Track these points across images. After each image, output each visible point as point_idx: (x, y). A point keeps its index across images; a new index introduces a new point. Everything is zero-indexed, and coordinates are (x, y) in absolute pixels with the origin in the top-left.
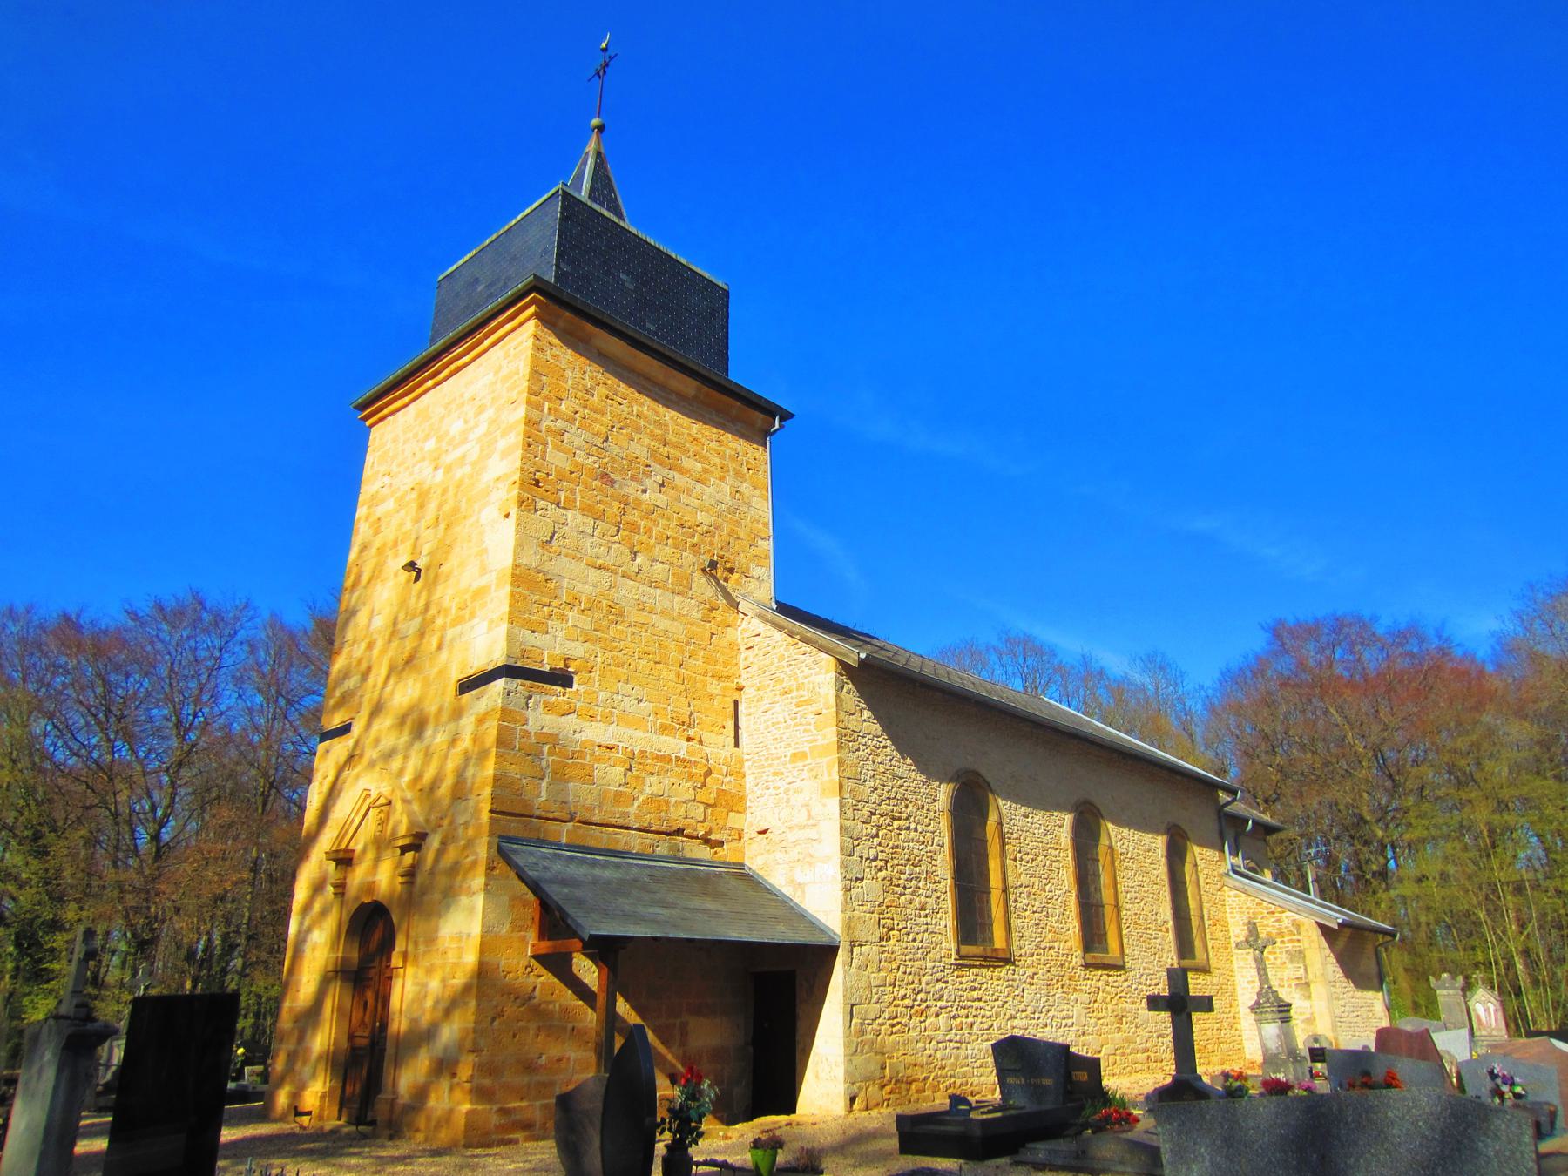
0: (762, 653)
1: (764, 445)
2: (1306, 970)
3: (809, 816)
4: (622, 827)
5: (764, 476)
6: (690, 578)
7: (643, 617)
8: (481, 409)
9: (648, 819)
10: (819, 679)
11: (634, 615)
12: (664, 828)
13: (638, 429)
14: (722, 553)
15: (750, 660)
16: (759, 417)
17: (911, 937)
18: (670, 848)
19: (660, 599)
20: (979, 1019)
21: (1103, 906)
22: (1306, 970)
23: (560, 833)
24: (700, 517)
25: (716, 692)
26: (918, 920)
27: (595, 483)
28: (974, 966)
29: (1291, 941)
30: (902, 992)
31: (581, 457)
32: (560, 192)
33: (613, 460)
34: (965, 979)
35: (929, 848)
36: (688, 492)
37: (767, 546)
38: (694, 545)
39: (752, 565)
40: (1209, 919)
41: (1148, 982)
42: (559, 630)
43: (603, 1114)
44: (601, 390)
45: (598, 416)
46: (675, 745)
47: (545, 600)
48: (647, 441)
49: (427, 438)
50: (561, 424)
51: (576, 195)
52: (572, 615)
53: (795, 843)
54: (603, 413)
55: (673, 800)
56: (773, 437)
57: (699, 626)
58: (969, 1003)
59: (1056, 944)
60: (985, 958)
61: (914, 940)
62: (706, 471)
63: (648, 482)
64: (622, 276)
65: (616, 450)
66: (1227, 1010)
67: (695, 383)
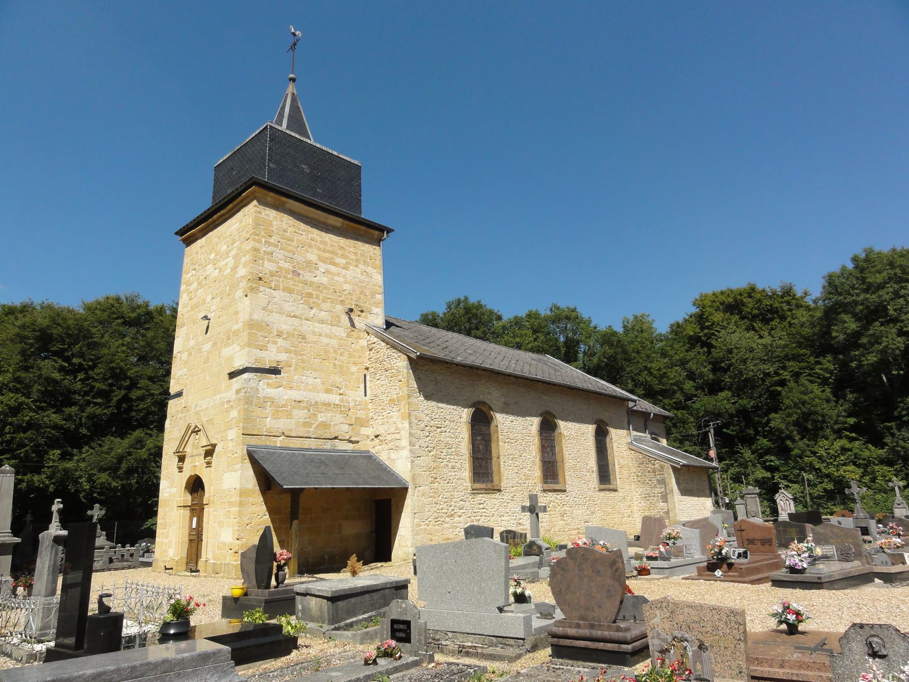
0: (376, 352)
1: (379, 246)
2: (666, 489)
3: (397, 429)
4: (307, 438)
5: (379, 262)
6: (339, 317)
7: (315, 338)
8: (234, 241)
9: (320, 433)
10: (400, 364)
11: (310, 338)
12: (328, 436)
13: (310, 246)
14: (357, 303)
15: (372, 354)
16: (376, 233)
17: (446, 482)
18: (331, 446)
19: (326, 329)
20: (483, 517)
21: (557, 462)
22: (666, 489)
23: (276, 442)
24: (345, 286)
25: (354, 371)
26: (450, 474)
27: (289, 276)
28: (481, 494)
29: (659, 475)
30: (441, 506)
31: (282, 264)
32: (269, 127)
33: (298, 263)
34: (475, 500)
35: (457, 440)
36: (338, 275)
37: (380, 297)
38: (342, 301)
39: (373, 308)
40: (619, 465)
41: (580, 497)
42: (272, 348)
43: (256, 561)
44: (292, 229)
45: (290, 243)
46: (335, 398)
47: (266, 335)
48: (316, 252)
49: (211, 253)
50: (270, 249)
51: (279, 128)
52: (280, 341)
53: (391, 441)
54: (293, 241)
55: (332, 423)
56: (384, 242)
57: (345, 340)
58: (478, 510)
59: (527, 482)
60: (486, 490)
61: (448, 483)
62: (347, 263)
63: (318, 272)
64: (303, 166)
65: (300, 258)
66: (627, 509)
67: (341, 220)
